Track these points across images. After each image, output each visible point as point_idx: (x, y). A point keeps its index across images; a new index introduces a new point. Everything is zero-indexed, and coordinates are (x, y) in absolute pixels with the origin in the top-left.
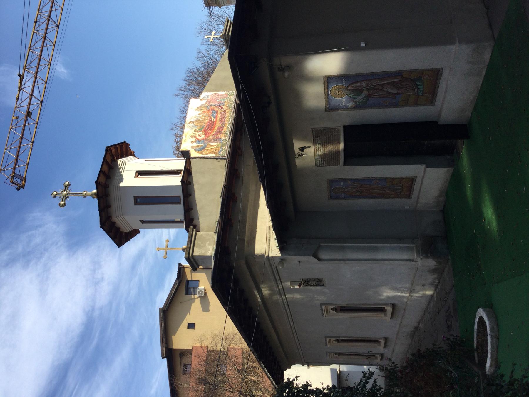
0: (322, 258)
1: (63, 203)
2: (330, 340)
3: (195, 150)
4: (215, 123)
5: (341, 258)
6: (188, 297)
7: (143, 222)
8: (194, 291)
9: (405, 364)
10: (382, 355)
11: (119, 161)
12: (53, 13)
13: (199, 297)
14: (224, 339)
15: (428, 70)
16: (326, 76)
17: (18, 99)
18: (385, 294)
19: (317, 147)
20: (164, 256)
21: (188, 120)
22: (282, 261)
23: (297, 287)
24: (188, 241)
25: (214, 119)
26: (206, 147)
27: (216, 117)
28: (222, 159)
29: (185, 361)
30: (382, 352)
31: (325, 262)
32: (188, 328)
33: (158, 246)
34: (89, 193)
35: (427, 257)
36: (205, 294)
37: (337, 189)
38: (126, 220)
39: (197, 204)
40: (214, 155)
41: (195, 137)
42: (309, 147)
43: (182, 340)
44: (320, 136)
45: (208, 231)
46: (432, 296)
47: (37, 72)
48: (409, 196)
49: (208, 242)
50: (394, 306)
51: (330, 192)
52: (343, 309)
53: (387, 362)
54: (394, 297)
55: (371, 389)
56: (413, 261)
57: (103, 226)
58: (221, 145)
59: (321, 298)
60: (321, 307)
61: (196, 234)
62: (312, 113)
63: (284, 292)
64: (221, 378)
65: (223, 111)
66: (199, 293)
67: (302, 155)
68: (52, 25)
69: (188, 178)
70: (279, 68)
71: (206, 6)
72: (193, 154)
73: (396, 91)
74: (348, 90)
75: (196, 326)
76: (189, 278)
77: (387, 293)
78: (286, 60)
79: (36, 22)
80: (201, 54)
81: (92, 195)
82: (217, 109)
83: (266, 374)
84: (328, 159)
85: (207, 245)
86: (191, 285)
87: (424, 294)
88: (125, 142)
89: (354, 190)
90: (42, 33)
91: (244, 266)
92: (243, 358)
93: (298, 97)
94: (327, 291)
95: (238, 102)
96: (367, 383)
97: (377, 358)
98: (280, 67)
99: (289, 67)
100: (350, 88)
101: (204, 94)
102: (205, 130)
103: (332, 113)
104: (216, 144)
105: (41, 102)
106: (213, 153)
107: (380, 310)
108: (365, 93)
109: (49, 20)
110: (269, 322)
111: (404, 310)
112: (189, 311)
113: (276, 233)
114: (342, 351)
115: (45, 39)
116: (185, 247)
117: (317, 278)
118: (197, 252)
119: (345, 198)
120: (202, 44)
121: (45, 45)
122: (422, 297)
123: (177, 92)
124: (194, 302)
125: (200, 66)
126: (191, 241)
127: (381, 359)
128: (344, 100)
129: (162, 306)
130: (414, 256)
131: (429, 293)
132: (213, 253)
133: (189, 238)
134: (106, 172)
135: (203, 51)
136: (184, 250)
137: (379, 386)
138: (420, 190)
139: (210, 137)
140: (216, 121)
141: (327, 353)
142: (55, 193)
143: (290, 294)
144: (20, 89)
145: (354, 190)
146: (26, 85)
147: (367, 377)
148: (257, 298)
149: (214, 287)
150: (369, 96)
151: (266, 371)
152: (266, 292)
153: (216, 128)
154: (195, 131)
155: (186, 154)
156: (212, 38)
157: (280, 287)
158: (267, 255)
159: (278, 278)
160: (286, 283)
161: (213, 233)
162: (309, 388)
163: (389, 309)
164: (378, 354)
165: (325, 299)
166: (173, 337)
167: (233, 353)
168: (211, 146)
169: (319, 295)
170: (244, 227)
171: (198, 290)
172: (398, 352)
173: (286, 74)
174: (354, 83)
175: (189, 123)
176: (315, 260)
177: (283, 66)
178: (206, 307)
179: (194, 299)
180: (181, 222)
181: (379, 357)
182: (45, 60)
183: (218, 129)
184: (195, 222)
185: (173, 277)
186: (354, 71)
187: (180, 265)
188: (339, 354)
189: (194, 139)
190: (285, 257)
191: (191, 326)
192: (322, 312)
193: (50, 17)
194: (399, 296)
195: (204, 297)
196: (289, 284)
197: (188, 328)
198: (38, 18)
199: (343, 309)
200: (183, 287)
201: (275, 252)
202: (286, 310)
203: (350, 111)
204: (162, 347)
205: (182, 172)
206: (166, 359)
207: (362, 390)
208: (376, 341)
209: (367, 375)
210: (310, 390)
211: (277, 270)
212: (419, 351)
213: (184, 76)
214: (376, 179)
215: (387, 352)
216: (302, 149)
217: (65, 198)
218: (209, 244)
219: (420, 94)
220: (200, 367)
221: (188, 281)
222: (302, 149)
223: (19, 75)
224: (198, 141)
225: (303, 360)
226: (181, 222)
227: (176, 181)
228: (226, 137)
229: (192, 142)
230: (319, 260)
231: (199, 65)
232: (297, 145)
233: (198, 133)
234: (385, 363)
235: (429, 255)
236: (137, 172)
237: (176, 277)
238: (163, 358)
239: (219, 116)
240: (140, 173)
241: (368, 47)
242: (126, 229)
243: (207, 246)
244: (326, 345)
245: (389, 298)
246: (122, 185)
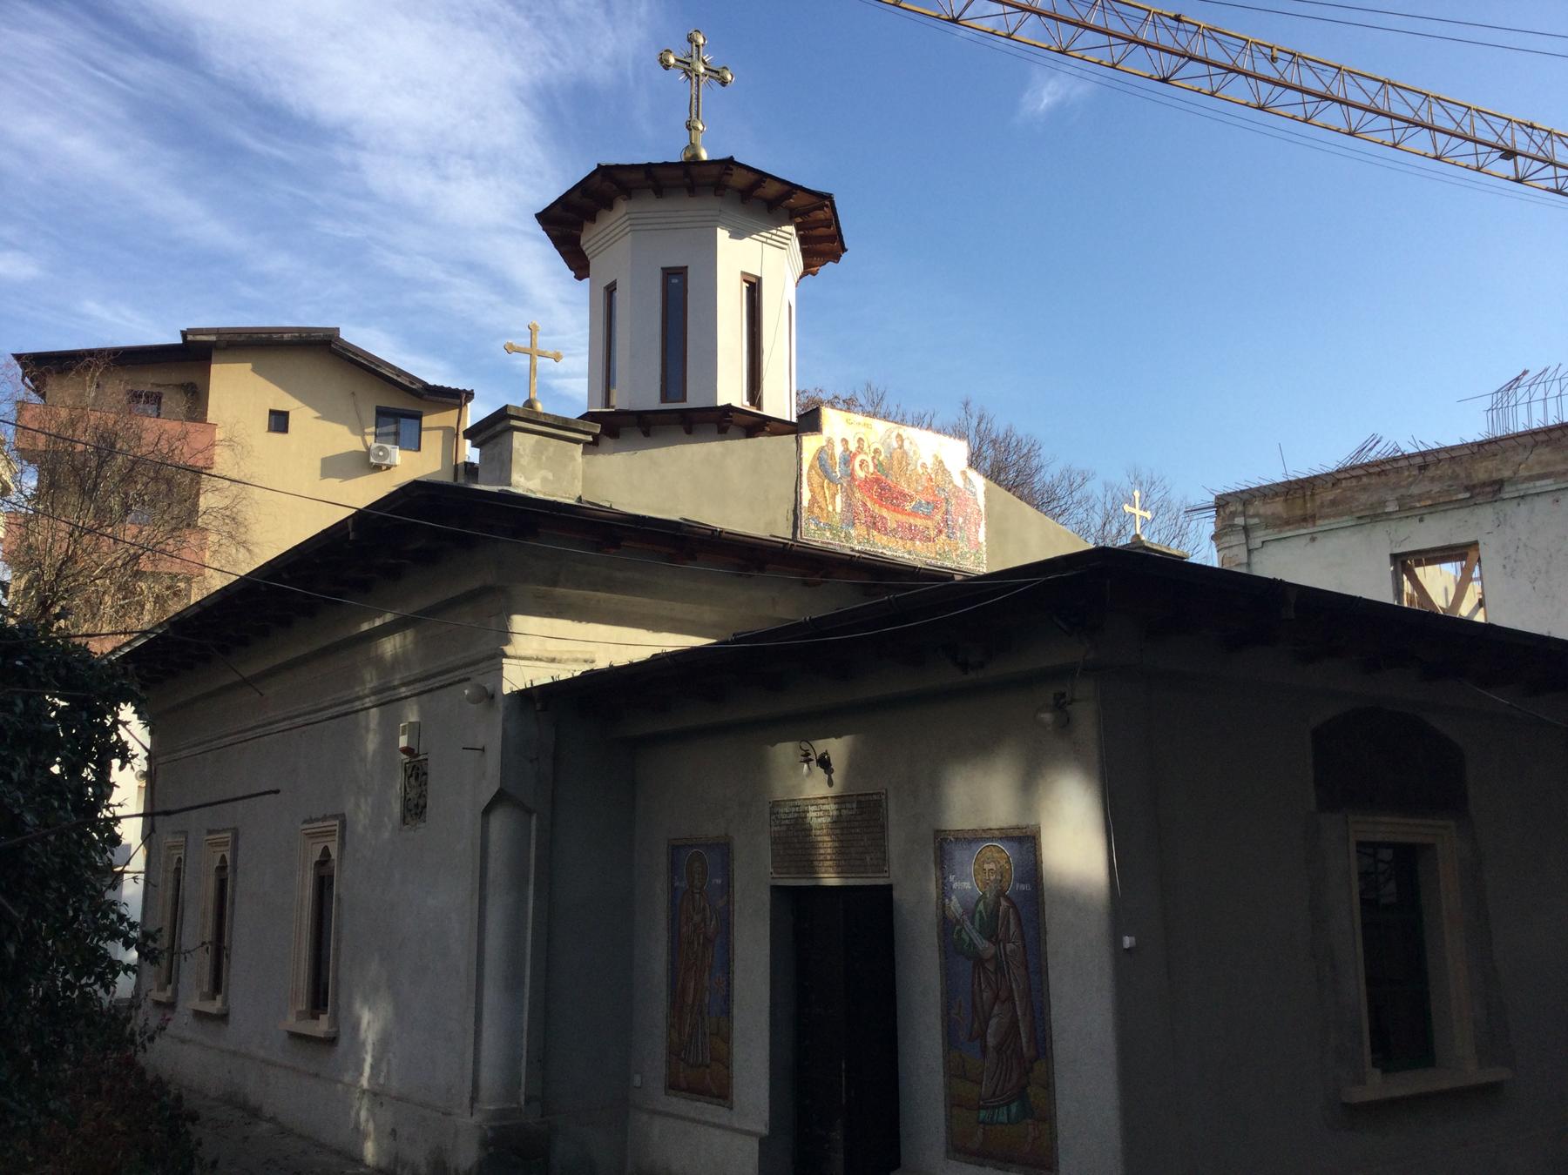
0: (492, 818)
1: (672, 60)
2: (226, 844)
3: (821, 450)
4: (897, 508)
5: (491, 874)
6: (371, 415)
7: (611, 290)
8: (387, 434)
9: (150, 1077)
10: (171, 1005)
11: (791, 229)
12: (1297, 96)
13: (368, 449)
14: (233, 520)
15: (1053, 1136)
16: (1039, 832)
18: (366, 1017)
19: (831, 807)
20: (511, 345)
21: (909, 432)
22: (489, 696)
23: (403, 741)
24: (556, 418)
25: (908, 507)
26: (831, 481)
27: (914, 514)
28: (795, 526)
29: (174, 402)
30: (179, 1008)
31: (479, 826)
32: (272, 412)
33: (537, 335)
34: (699, 139)
35: (484, 1144)
36: (377, 468)
37: (701, 867)
38: (616, 239)
39: (664, 450)
40: (805, 503)
41: (860, 449)
42: (830, 783)
43: (237, 393)
44: (862, 816)
45: (586, 480)
46: (359, 1161)
47: (1040, 14)
48: (673, 1086)
49: (550, 476)
50: (331, 1041)
51: (691, 846)
52: (323, 884)
53: (154, 1023)
54: (357, 1045)
55: (106, 956)
56: (474, 1099)
57: (603, 171)
58: (832, 526)
59: (361, 814)
60: (335, 817)
61: (577, 441)
62: (930, 794)
63: (388, 700)
64: (115, 503)
65: (933, 533)
66: (381, 449)
67: (808, 761)
68: (1168, 63)
69: (738, 425)
70: (1063, 695)
71: (1217, 498)
72: (811, 443)
73: (991, 1041)
74: (998, 897)
75: (278, 437)
76: (427, 421)
77: (370, 1021)
78: (1086, 717)
79: (1177, 18)
80: (1079, 480)
81: (692, 146)
82: (938, 517)
83: (128, 644)
84: (793, 838)
85: (543, 473)
86: (406, 425)
87: (365, 1136)
88: (844, 250)
89: (697, 918)
90: (1145, 35)
91: (474, 584)
92: (174, 577)
93: (978, 747)
94: (386, 835)
95: (958, 578)
96: (127, 945)
97: (162, 988)
98: (1068, 698)
99: (1065, 724)
100: (1004, 903)
101: (979, 482)
102: (877, 480)
103: (931, 852)
104: (838, 510)
105: (955, 21)
106: (813, 500)
107: (319, 999)
108: (983, 945)
109: (1183, 56)
110: (291, 654)
111: (317, 1075)
112: (328, 415)
113: (574, 679)
114: (187, 879)
115: (1131, 41)
116: (540, 407)
117: (429, 803)
118: (522, 443)
119: (673, 890)
120: (1107, 486)
121: (1113, 40)
122: (357, 1128)
123: (975, 409)
124: (354, 433)
125: (1048, 479)
126: (557, 427)
127: (158, 1004)
128: (967, 885)
130: (488, 1105)
131: (370, 1151)
132: (520, 491)
133: (566, 420)
134: (759, 192)
135: (1088, 486)
136: (529, 404)
137: (113, 983)
138: (693, 1120)
139: (858, 495)
140: (903, 512)
141: (185, 833)
142: (701, 41)
143: (379, 724)
145: (697, 918)
147: (145, 945)
148: (372, 619)
149: (415, 495)
150: (979, 962)
151: (137, 644)
152: (390, 646)
153: (885, 513)
154: (876, 451)
155: (809, 421)
156: (1142, 513)
157: (404, 691)
158: (508, 650)
159: (429, 685)
160: (415, 708)
161: (578, 492)
162: (116, 763)
163: (321, 1027)
164: (175, 991)
165: (360, 828)
166: (249, 366)
167: (193, 540)
168: (833, 496)
169: (372, 810)
170: (594, 587)
171: (389, 447)
172: (181, 1055)
173: (1047, 717)
174: (1019, 920)
175: (899, 436)
176: (486, 797)
177: (1069, 708)
178: (336, 467)
179: (363, 434)
180: (607, 404)
181: (163, 997)
182: (1074, 39)
183: (882, 518)
184: (607, 442)
185: (434, 373)
186: (1054, 918)
187: (469, 395)
188: (178, 870)
189: (853, 447)
190: (501, 705)
191: (279, 421)
192: (318, 820)
193: (1191, 58)
194: (364, 1060)
195: (367, 464)
196: (413, 717)
197: (272, 412)
198: (1188, 27)
199: (323, 884)
200: (403, 403)
201: (517, 676)
202: (331, 707)
203: (938, 898)
204: (217, 332)
205: (754, 410)
206: (179, 340)
207: (106, 928)
208: (217, 985)
209: (150, 943)
210: (110, 767)
211: (460, 681)
212: (194, 1118)
213: (1020, 432)
214: (729, 984)
215: (181, 1021)
216: (825, 763)
217: (689, 71)
218: (544, 480)
219: (983, 1114)
220: (149, 438)
221: (418, 417)
222: (825, 763)
224: (848, 459)
225: (161, 760)
226: (607, 404)
227: (731, 391)
228: (856, 541)
229: (845, 441)
230: (487, 812)
231: (1049, 474)
232: (836, 748)
233: (869, 459)
234: (146, 1017)
235: (491, 1149)
236: (759, 279)
237: (431, 381)
238: (184, 334)
239: (919, 522)
240: (754, 288)
241: (1121, 957)
242: (590, 240)
243: (539, 473)
244: (210, 832)
245: (356, 1027)
246: (722, 235)
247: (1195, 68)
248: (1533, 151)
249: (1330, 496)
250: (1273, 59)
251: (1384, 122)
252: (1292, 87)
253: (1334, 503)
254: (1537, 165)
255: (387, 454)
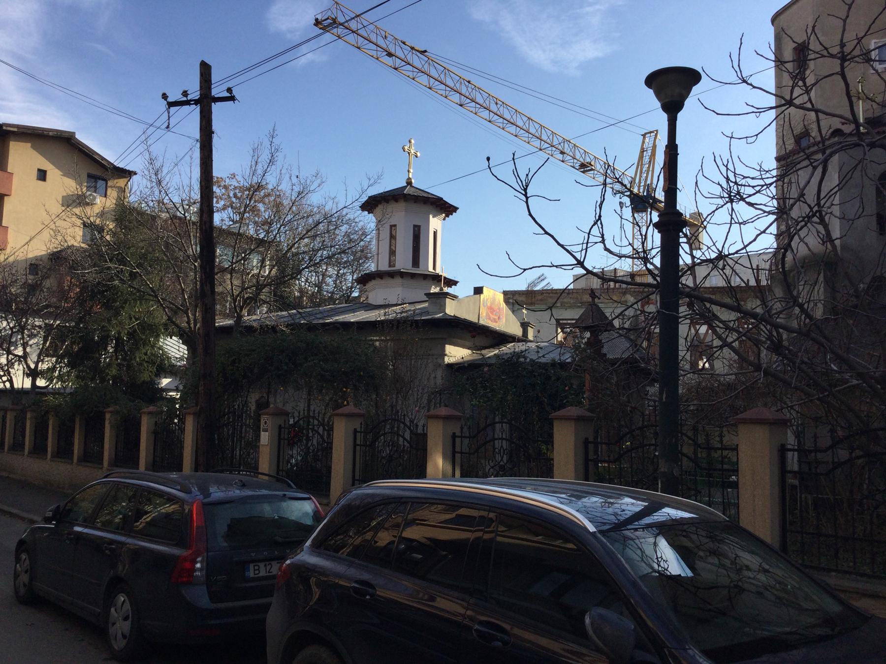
7: (393, 227)
12: (374, 47)
17: (404, 43)
32: (39, 170)
76: (110, 183)
79: (469, 82)
86: (100, 183)
112: (67, 174)
129: (78, 136)
144: (412, 48)
146: (415, 57)
166: (29, 145)
191: (42, 175)
197: (39, 170)
204: (17, 126)
223: (425, 51)
240: (435, 233)
247: (409, 67)
248: (467, 94)
249: (540, 298)
250: (497, 104)
251: (443, 87)
252: (406, 59)
253: (541, 300)
254: (468, 101)
255: (95, 198)
